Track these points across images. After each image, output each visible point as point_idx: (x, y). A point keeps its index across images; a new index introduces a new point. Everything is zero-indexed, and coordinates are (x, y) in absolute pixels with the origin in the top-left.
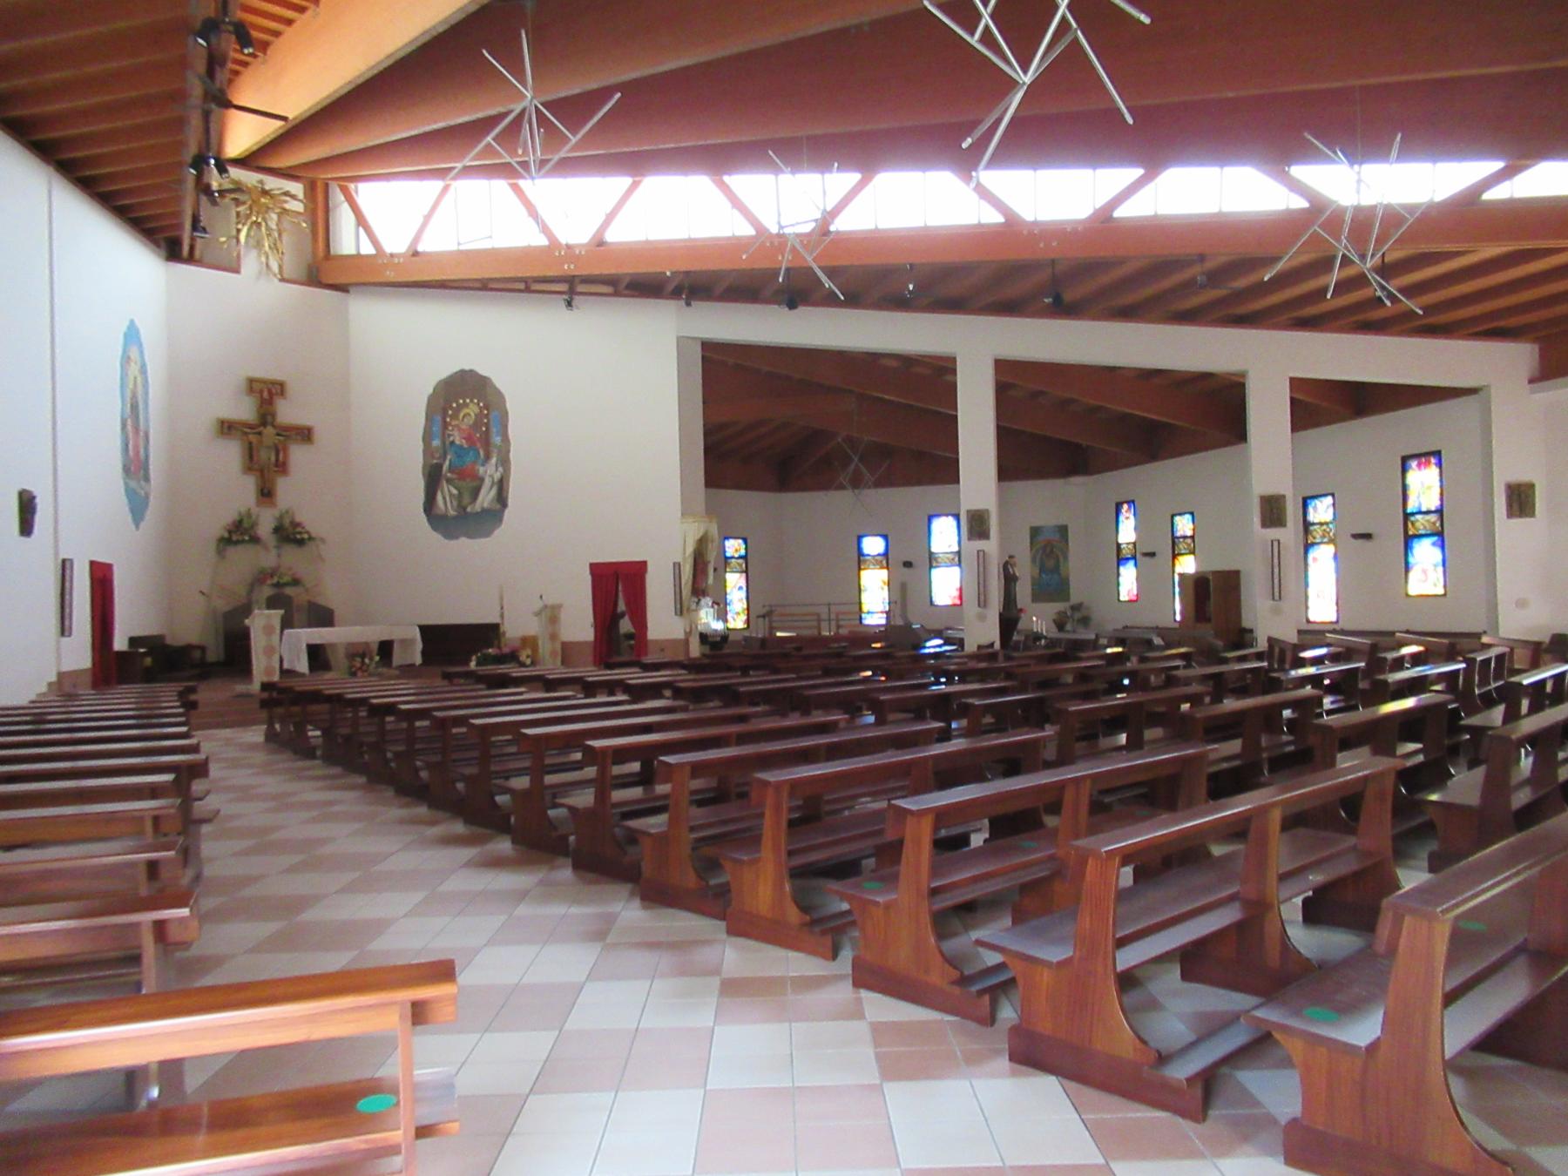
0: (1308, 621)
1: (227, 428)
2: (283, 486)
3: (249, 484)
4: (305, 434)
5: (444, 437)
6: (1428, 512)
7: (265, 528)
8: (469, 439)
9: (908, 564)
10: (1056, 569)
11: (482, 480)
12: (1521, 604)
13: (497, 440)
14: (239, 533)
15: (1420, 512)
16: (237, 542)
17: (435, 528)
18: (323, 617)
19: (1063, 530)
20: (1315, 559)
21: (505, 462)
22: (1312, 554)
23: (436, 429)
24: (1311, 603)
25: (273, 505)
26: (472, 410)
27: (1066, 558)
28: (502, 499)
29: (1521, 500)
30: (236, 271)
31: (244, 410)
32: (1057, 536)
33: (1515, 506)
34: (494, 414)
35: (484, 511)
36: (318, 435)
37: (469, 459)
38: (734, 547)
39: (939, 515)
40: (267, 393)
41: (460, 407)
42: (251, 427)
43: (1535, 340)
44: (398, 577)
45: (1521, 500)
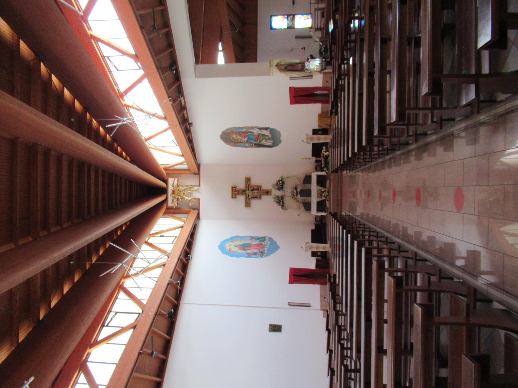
1: (247, 205)
2: (266, 186)
3: (265, 197)
4: (248, 180)
5: (245, 143)
7: (279, 193)
8: (245, 137)
11: (259, 134)
13: (244, 130)
14: (280, 201)
16: (283, 203)
17: (278, 145)
18: (307, 179)
21: (252, 128)
23: (242, 145)
25: (271, 191)
26: (234, 136)
28: (266, 129)
30: (199, 200)
31: (241, 199)
34: (235, 131)
35: (271, 133)
36: (248, 176)
37: (252, 137)
39: (274, 16)
40: (235, 192)
41: (235, 139)
42: (246, 198)
44: (293, 154)
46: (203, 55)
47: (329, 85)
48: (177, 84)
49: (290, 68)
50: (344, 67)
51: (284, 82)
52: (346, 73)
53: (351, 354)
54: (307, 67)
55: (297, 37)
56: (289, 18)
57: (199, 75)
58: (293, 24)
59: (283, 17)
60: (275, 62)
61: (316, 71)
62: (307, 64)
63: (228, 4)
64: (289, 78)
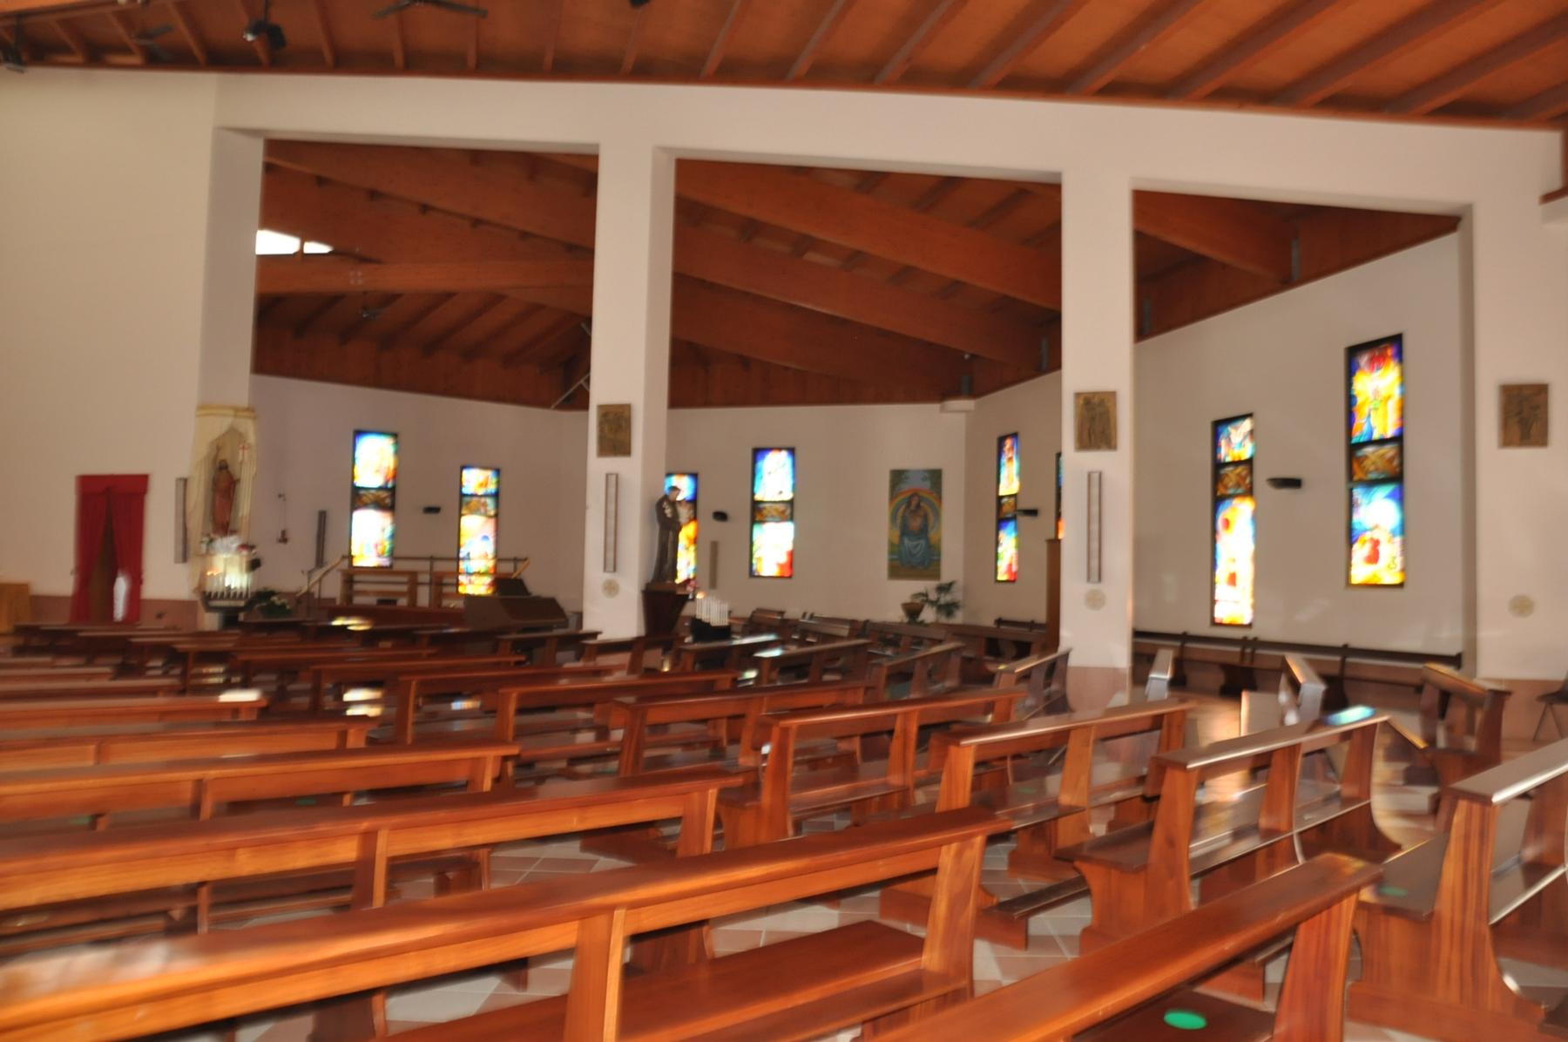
0: (1214, 623)
6: (1382, 442)
9: (721, 516)
10: (923, 532)
12: (1522, 606)
15: (1370, 442)
19: (935, 476)
20: (1227, 523)
22: (1226, 512)
24: (463, 540)
27: (937, 515)
29: (1526, 414)
32: (927, 485)
33: (1516, 431)
38: (475, 481)
43: (1551, 122)
45: (1526, 414)
46: (298, 178)
47: (148, 622)
48: (196, 51)
49: (223, 484)
50: (215, 673)
51: (170, 464)
52: (194, 682)
53: (356, 753)
54: (221, 542)
55: (323, 516)
56: (384, 494)
57: (228, 133)
58: (365, 506)
59: (391, 474)
60: (249, 428)
61: (203, 576)
62: (232, 542)
63: (449, 295)
64: (184, 473)
